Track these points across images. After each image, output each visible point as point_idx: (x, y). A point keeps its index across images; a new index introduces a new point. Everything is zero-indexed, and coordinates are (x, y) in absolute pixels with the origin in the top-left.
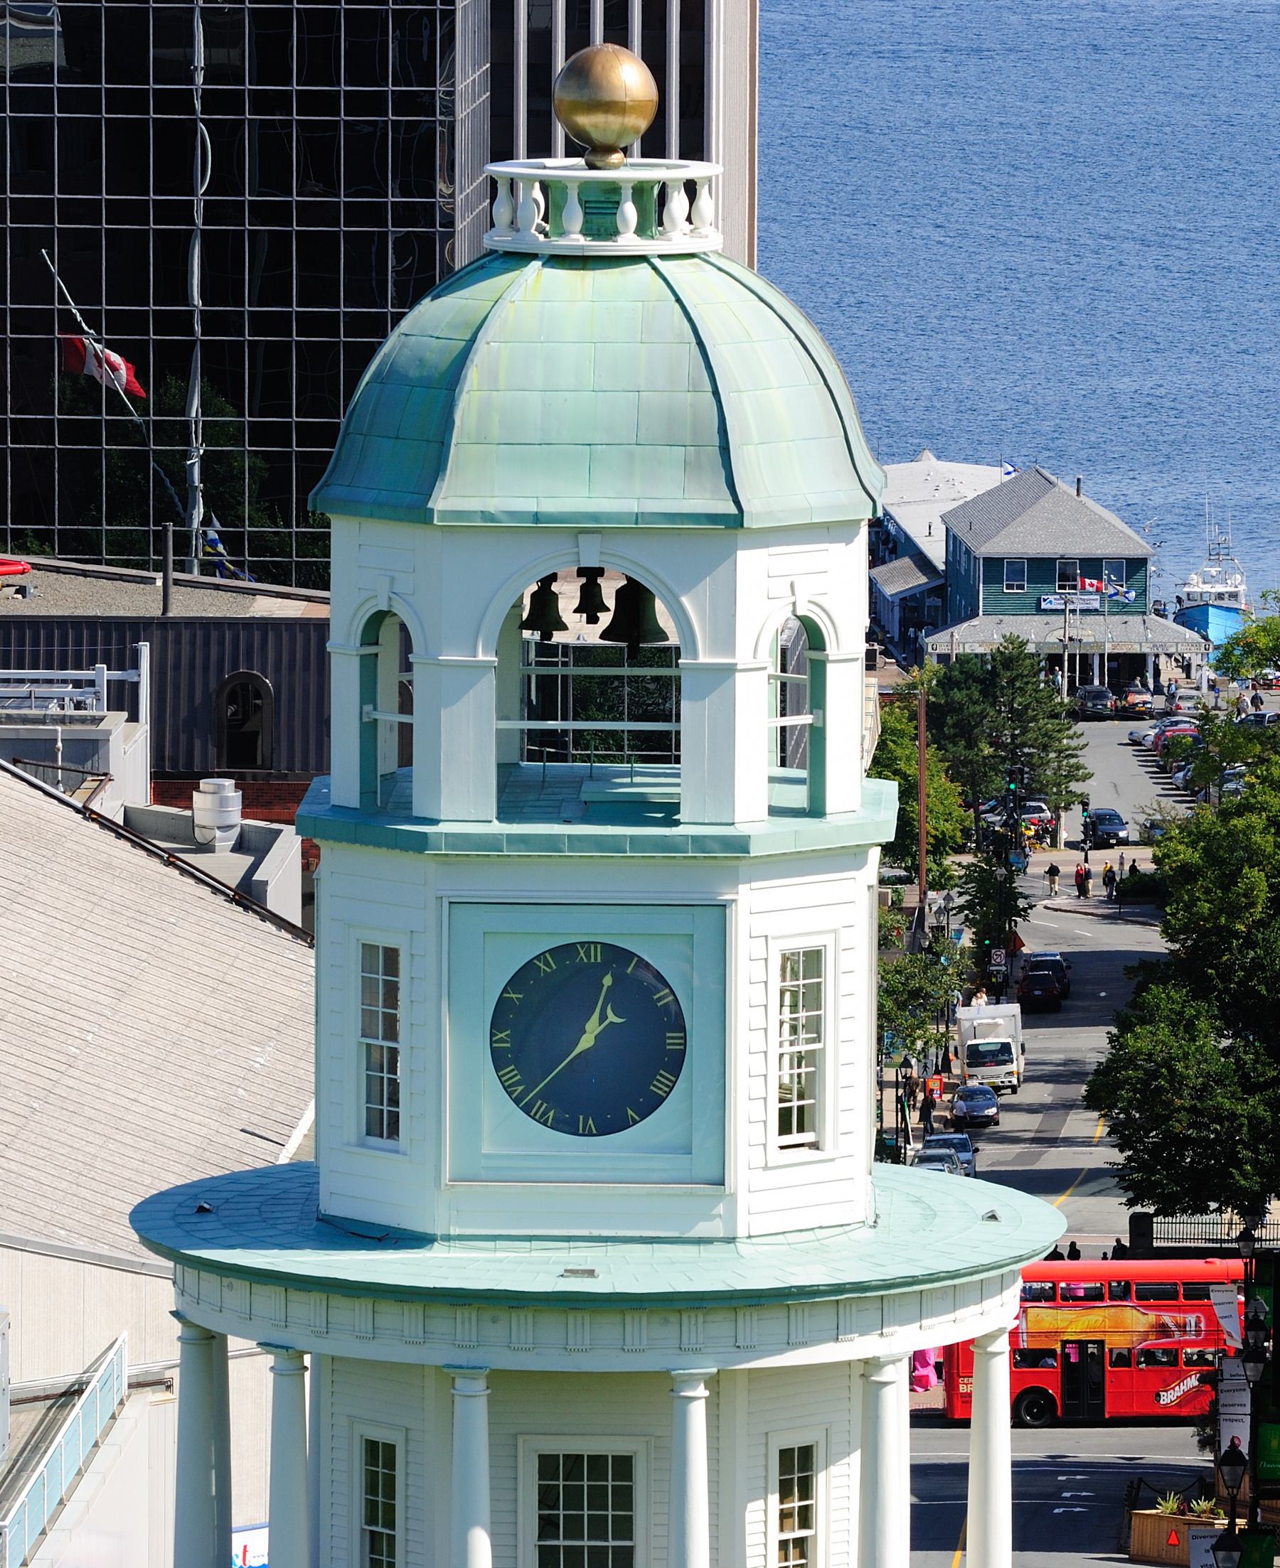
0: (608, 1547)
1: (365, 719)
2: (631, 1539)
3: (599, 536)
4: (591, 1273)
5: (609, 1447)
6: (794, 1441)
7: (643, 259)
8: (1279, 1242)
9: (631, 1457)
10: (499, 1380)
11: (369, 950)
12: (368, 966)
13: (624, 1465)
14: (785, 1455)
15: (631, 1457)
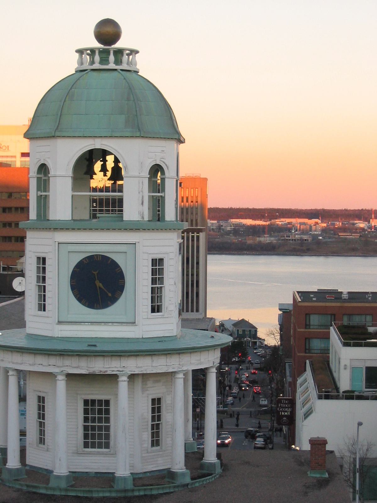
0: (102, 426)
1: (38, 195)
2: (109, 423)
3: (217, 349)
4: (95, 346)
5: (103, 397)
6: (156, 396)
7: (116, 70)
8: (375, 223)
9: (84, 400)
10: (70, 376)
11: (39, 258)
12: (38, 263)
13: (107, 402)
14: (153, 400)
15: (84, 400)
